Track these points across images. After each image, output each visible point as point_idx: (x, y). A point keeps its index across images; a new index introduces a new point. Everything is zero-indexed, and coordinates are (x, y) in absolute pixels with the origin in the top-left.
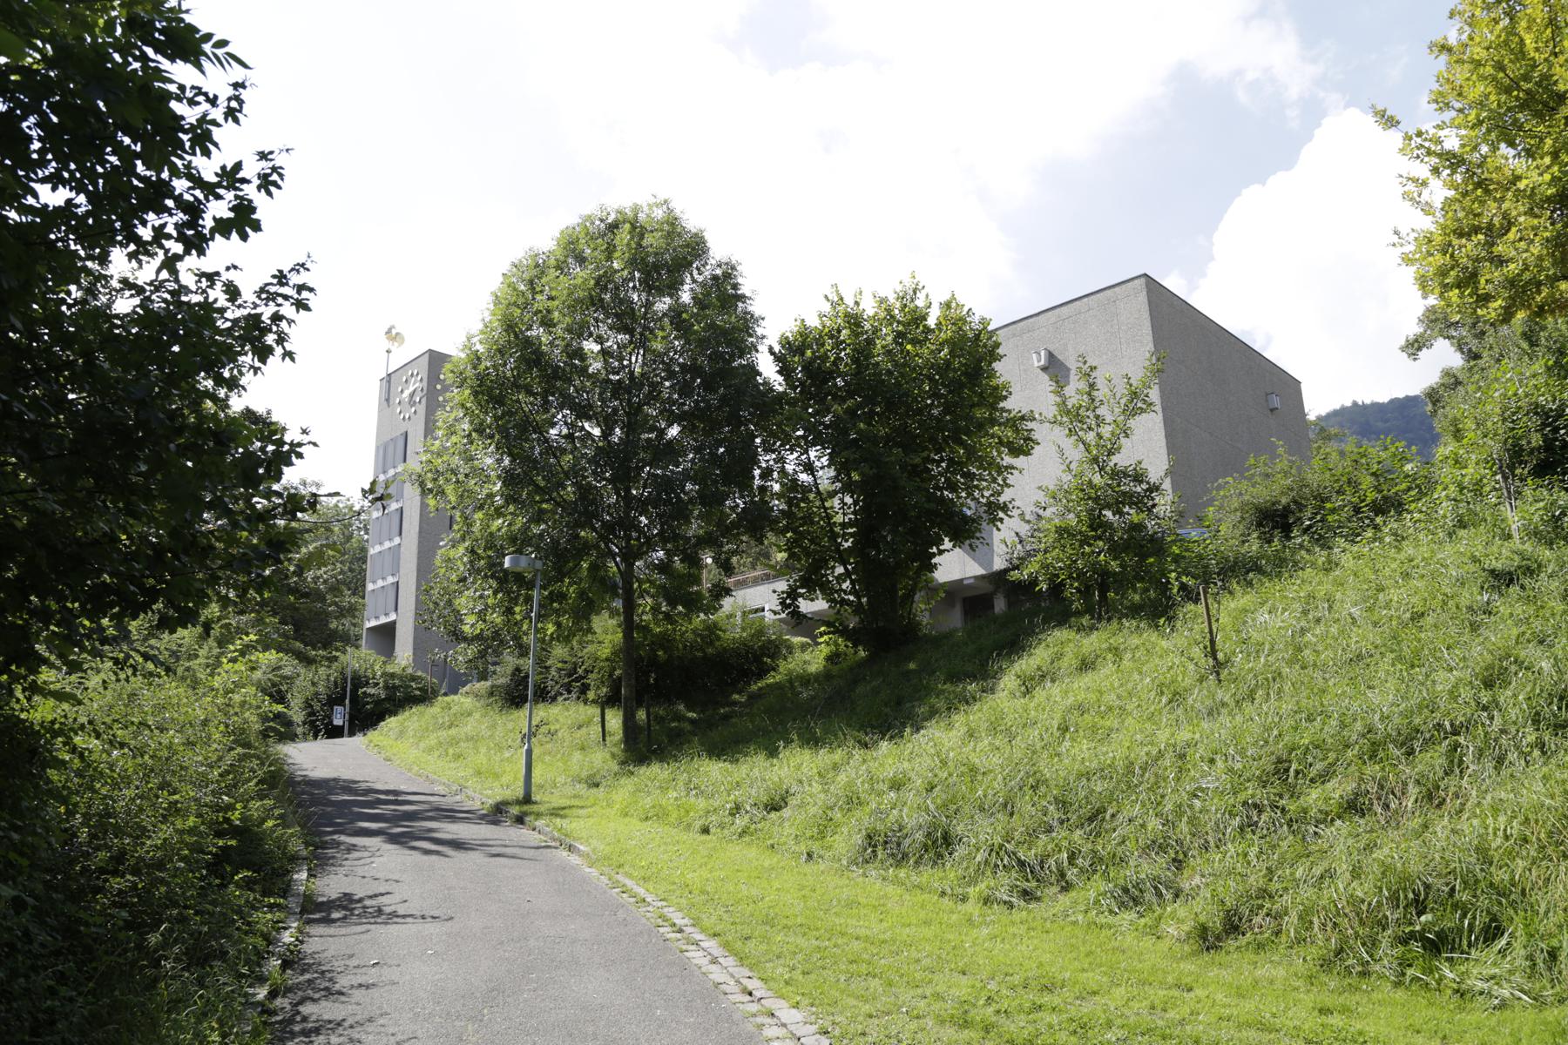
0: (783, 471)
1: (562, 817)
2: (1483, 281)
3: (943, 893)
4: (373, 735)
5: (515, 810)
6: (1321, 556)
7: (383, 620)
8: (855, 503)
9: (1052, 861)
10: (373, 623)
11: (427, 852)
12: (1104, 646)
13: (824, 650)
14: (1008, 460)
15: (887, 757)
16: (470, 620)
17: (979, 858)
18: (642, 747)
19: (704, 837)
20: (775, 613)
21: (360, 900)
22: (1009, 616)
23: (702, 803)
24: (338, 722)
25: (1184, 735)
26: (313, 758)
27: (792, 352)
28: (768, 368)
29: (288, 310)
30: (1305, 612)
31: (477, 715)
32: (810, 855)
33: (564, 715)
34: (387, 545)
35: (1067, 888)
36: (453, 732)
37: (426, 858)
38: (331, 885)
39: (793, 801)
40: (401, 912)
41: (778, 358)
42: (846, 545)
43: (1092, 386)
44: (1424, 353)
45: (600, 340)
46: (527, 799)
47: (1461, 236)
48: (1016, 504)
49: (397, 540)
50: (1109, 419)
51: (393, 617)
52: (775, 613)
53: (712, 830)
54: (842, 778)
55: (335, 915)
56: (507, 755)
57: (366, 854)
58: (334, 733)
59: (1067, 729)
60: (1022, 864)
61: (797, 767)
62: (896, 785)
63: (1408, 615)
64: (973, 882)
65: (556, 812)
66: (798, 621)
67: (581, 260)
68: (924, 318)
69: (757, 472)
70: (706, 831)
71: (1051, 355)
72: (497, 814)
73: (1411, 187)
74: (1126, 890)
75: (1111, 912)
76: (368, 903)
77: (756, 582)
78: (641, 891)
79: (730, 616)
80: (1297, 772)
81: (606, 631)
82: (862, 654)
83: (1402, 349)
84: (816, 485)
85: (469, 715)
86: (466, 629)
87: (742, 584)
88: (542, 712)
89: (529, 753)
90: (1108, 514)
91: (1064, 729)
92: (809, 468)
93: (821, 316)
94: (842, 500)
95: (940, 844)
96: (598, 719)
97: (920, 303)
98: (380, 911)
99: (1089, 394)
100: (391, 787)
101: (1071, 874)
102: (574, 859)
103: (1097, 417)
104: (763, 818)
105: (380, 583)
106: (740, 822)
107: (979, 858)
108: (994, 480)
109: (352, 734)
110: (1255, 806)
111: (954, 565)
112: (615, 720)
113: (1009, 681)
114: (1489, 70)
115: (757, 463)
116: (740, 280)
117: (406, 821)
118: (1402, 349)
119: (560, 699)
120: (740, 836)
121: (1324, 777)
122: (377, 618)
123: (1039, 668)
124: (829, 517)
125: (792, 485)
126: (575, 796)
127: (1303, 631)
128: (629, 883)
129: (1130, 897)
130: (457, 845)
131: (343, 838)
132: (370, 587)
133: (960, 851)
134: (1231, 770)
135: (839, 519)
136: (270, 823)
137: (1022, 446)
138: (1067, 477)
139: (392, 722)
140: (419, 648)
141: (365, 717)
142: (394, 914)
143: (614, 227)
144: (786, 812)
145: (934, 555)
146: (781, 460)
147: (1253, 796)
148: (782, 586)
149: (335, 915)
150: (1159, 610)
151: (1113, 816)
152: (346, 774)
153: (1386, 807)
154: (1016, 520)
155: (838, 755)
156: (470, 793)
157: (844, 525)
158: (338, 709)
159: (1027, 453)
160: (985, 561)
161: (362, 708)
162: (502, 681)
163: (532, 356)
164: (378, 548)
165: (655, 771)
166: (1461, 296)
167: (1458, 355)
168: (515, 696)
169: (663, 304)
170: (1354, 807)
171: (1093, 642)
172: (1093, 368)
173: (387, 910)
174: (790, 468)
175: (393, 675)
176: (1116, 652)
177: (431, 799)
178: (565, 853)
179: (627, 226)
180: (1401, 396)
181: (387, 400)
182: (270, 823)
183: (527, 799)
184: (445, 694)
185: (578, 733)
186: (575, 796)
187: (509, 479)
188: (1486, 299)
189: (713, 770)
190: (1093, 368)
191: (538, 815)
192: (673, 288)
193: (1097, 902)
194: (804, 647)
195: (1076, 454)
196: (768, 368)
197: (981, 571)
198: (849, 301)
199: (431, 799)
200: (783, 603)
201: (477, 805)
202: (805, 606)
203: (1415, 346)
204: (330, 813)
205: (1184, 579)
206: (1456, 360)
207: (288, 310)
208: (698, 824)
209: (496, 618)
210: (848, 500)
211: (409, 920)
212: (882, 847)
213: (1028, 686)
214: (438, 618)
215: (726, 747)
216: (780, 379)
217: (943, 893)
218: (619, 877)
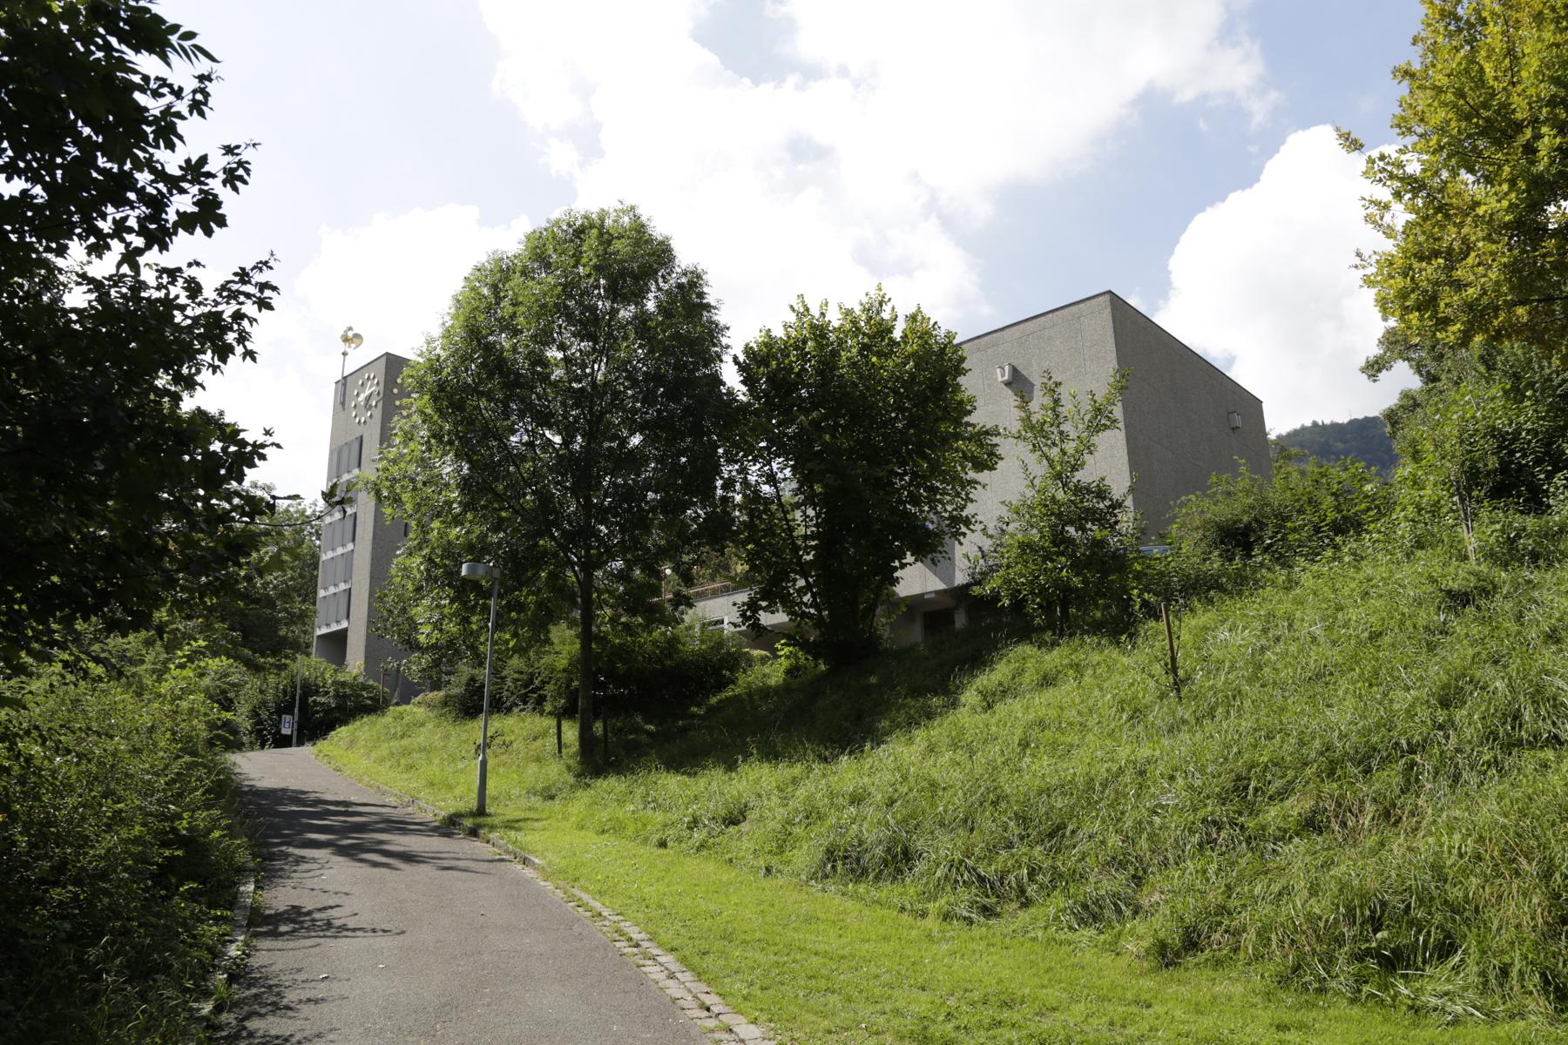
0: (745, 483)
1: (518, 829)
2: (1442, 305)
3: (903, 909)
4: (322, 745)
5: (468, 823)
6: (1281, 575)
7: (335, 628)
8: (818, 516)
9: (1012, 877)
10: (324, 630)
11: (375, 864)
12: (1066, 662)
13: (784, 664)
14: (972, 475)
15: (847, 772)
16: (426, 629)
17: (938, 874)
18: (596, 761)
19: (662, 851)
20: (735, 625)
21: (309, 913)
22: (971, 631)
23: (659, 817)
24: (286, 731)
25: (1145, 752)
26: (261, 768)
27: (757, 362)
28: (731, 377)
29: (250, 309)
30: (1265, 631)
31: (430, 726)
32: (768, 870)
33: (518, 726)
34: (340, 551)
35: (1027, 904)
36: (405, 742)
37: (376, 870)
38: (279, 898)
39: (751, 815)
40: (351, 924)
41: (742, 368)
42: (809, 557)
43: (1057, 402)
44: (1383, 375)
45: (562, 347)
46: (481, 811)
47: (1421, 259)
48: (978, 518)
49: (350, 546)
50: (1073, 435)
51: (344, 624)
52: (735, 625)
53: (670, 844)
54: (801, 793)
55: (283, 928)
56: (460, 766)
57: (315, 866)
58: (282, 742)
59: (1028, 745)
60: (982, 879)
61: (756, 780)
62: (856, 800)
63: (1366, 634)
64: (933, 897)
65: (511, 825)
66: (760, 635)
67: (548, 266)
68: (890, 330)
69: (719, 483)
70: (663, 844)
71: (1015, 371)
72: (449, 826)
73: (1373, 210)
74: (1085, 907)
75: (1070, 928)
76: (317, 916)
77: (715, 594)
78: (597, 905)
79: (690, 628)
80: (1256, 790)
81: (564, 641)
82: (823, 667)
83: (1363, 370)
84: (779, 497)
85: (422, 725)
86: (422, 639)
87: (702, 596)
88: (497, 723)
89: (484, 764)
90: (1071, 530)
91: (1024, 744)
92: (771, 479)
93: (786, 326)
94: (804, 513)
95: (899, 859)
96: (553, 731)
97: (886, 315)
98: (329, 925)
99: (1054, 410)
100: (341, 798)
101: (1031, 890)
102: (529, 872)
103: (1061, 433)
104: (722, 832)
105: (332, 590)
106: (698, 836)
107: (938, 874)
108: (958, 495)
109: (300, 743)
110: (1215, 823)
111: (915, 580)
112: (571, 733)
113: (970, 697)
114: (1450, 97)
115: (719, 473)
116: (705, 289)
117: (357, 833)
118: (1363, 370)
119: (516, 710)
120: (698, 850)
121: (1283, 794)
122: (328, 625)
123: (1000, 684)
124: (791, 529)
125: (754, 497)
126: (530, 809)
127: (1263, 649)
128: (585, 897)
129: (1090, 914)
130: (408, 857)
131: (291, 850)
132: (321, 593)
133: (920, 867)
134: (1191, 787)
135: (801, 531)
136: (216, 834)
137: (986, 460)
138: (1030, 493)
139: (342, 732)
140: (371, 656)
141: (315, 727)
142: (344, 928)
143: (580, 232)
144: (744, 827)
145: (896, 569)
146: (743, 471)
147: (1212, 813)
148: (742, 597)
149: (283, 928)
150: (1120, 627)
151: (1073, 832)
152: (294, 784)
153: (1344, 824)
154: (978, 534)
155: (798, 769)
156: (423, 804)
157: (806, 537)
158: (287, 718)
159: (992, 468)
160: (947, 576)
161: (312, 717)
162: (455, 691)
163: (495, 363)
164: (330, 554)
165: (612, 785)
166: (1421, 319)
167: (1417, 377)
168: (469, 706)
169: (626, 313)
170: (1311, 824)
171: (1054, 658)
172: (1058, 384)
173: (337, 923)
174: (752, 479)
175: (343, 684)
176: (1077, 668)
177: (383, 810)
178: (520, 867)
179: (595, 232)
180: (1361, 417)
181: (343, 403)
182: (216, 834)
183: (481, 811)
184: (397, 704)
185: (533, 745)
186: (530, 809)
187: (465, 485)
188: (1444, 323)
189: (671, 783)
190: (1058, 384)
191: (492, 828)
192: (638, 296)
193: (1056, 918)
194: (763, 660)
195: (1040, 470)
196: (731, 377)
197: (941, 586)
198: (815, 312)
199: (383, 810)
200: (743, 615)
201: (429, 817)
202: (766, 619)
203: (1374, 368)
204: (280, 824)
205: (1146, 596)
206: (1415, 383)
207: (250, 309)
208: (655, 838)
209: (452, 627)
210: (811, 512)
211: (359, 933)
212: (845, 863)
213: (989, 701)
214: (391, 627)
215: (684, 760)
216: (744, 389)
217: (903, 909)
218: (576, 891)
